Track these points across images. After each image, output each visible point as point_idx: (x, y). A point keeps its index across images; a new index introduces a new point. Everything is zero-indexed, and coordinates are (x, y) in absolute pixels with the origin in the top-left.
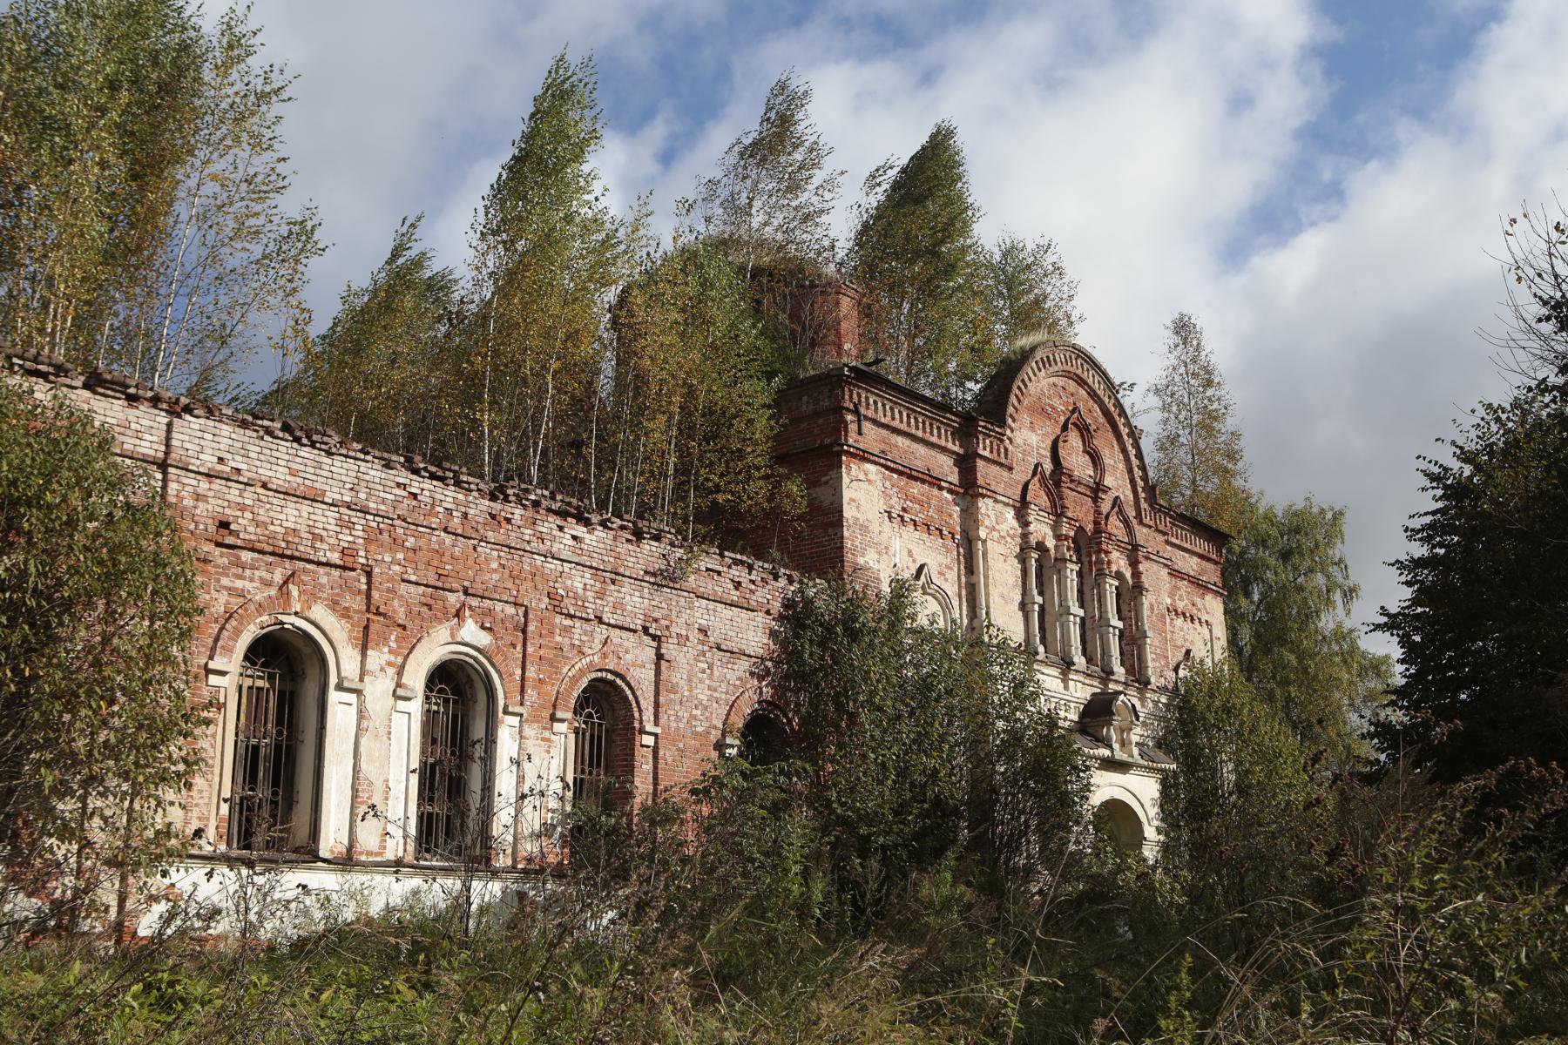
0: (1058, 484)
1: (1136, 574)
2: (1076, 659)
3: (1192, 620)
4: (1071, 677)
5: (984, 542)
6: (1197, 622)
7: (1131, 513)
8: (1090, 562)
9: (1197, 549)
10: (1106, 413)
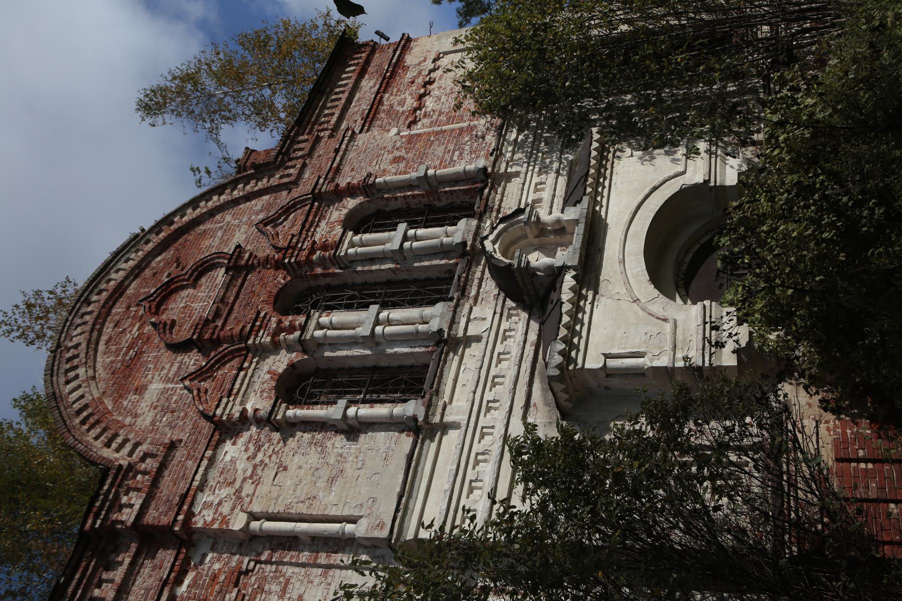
0: (216, 343)
1: (351, 191)
2: (457, 239)
3: (431, 82)
4: (460, 334)
5: (253, 516)
6: (433, 75)
7: (284, 198)
8: (324, 275)
9: (351, 82)
10: (163, 246)
